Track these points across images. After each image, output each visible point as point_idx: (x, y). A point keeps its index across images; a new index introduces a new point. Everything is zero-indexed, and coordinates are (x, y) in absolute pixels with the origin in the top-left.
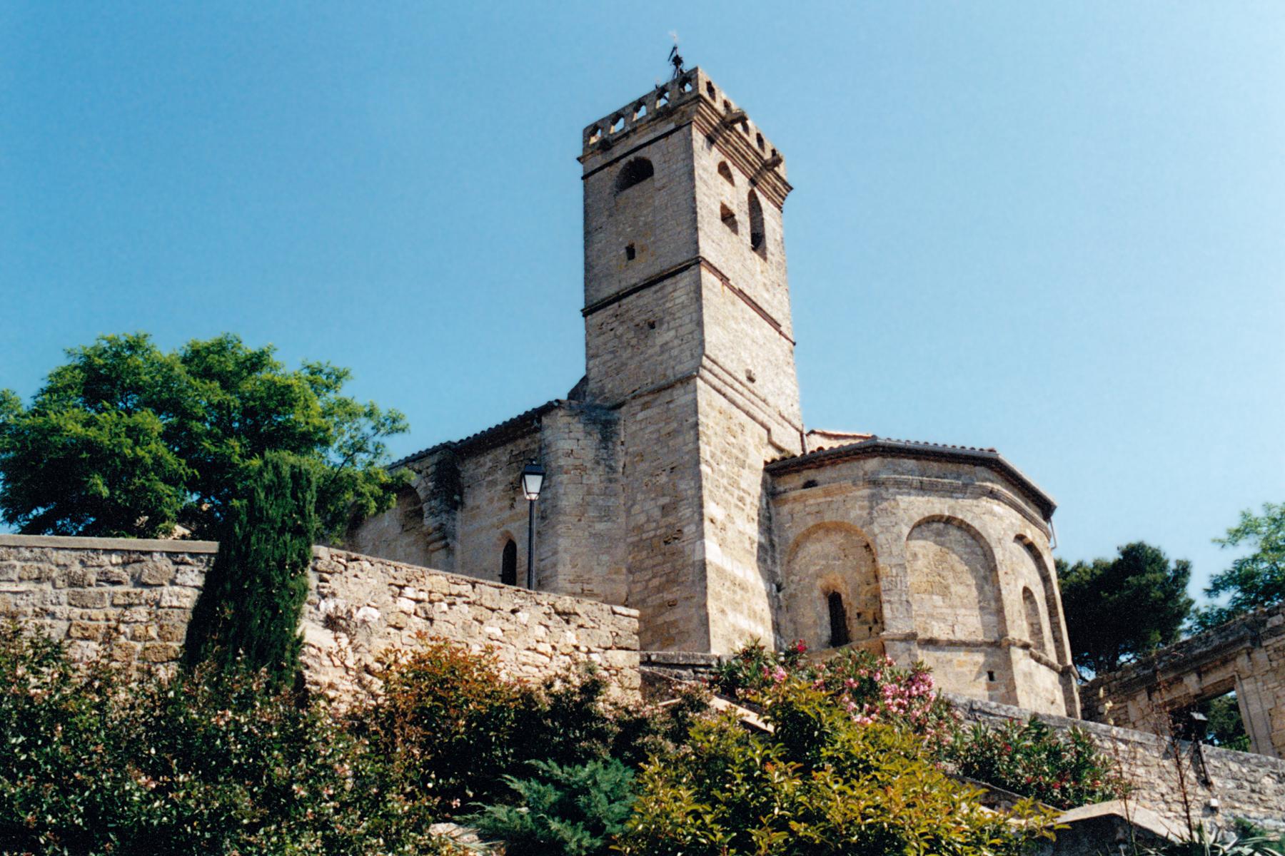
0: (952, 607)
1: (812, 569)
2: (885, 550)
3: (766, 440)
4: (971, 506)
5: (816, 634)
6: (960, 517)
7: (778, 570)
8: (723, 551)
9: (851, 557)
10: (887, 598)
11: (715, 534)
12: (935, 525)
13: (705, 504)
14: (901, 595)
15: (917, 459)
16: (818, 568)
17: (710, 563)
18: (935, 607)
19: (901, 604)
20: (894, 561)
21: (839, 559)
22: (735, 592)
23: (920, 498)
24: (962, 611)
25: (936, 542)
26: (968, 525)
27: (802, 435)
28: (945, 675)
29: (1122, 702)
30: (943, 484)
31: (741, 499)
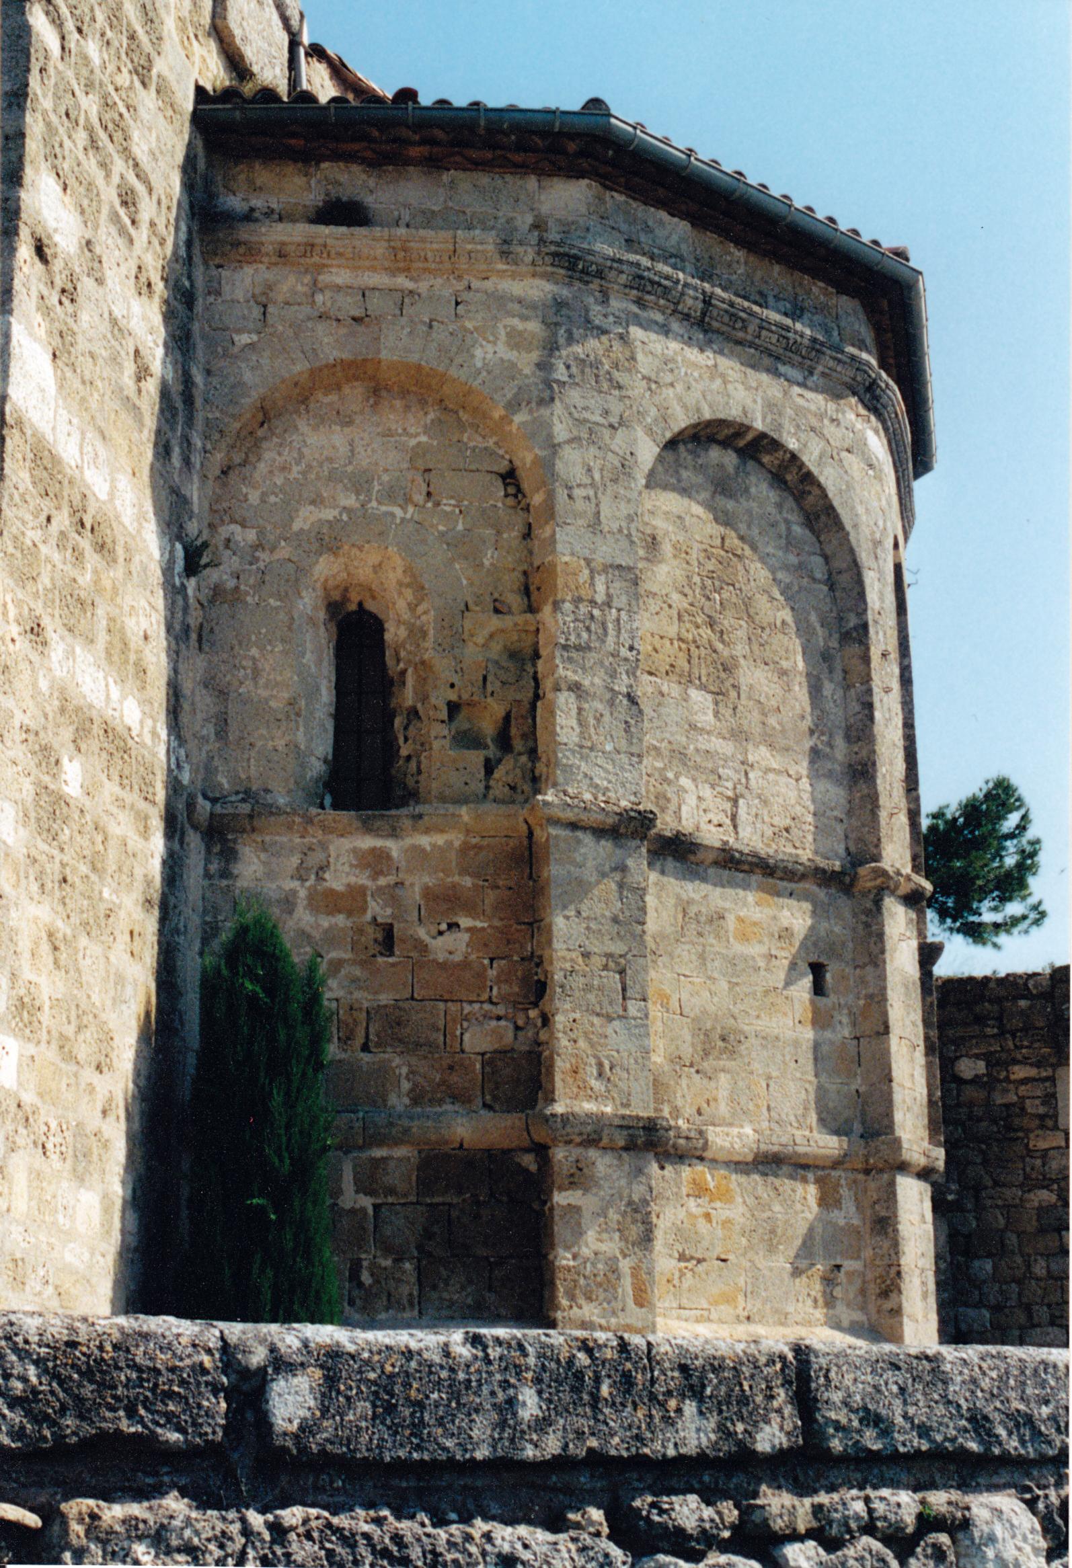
0: (739, 735)
1: (306, 518)
2: (580, 505)
3: (206, 20)
4: (821, 416)
5: (293, 746)
6: (792, 444)
7: (194, 492)
8: (61, 383)
9: (448, 505)
10: (573, 677)
11: (47, 311)
12: (715, 454)
13: (29, 173)
14: (613, 675)
15: (698, 221)
16: (329, 514)
17: (20, 423)
18: (693, 727)
19: (611, 703)
20: (606, 551)
21: (408, 500)
22: (78, 555)
23: (693, 354)
24: (760, 755)
25: (710, 507)
26: (808, 478)
27: (294, 44)
28: (702, 957)
29: (1038, 1065)
30: (764, 325)
31: (128, 199)
